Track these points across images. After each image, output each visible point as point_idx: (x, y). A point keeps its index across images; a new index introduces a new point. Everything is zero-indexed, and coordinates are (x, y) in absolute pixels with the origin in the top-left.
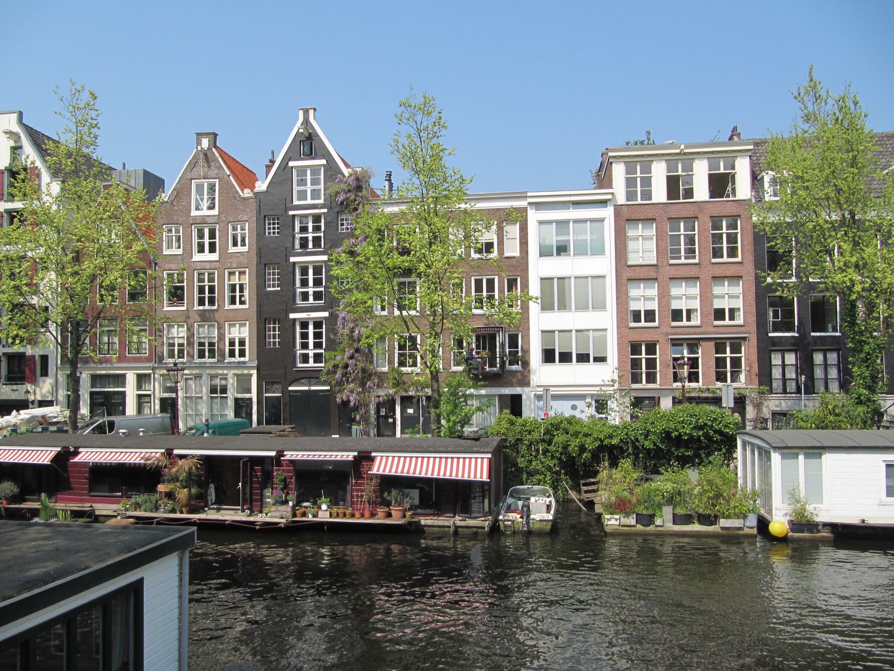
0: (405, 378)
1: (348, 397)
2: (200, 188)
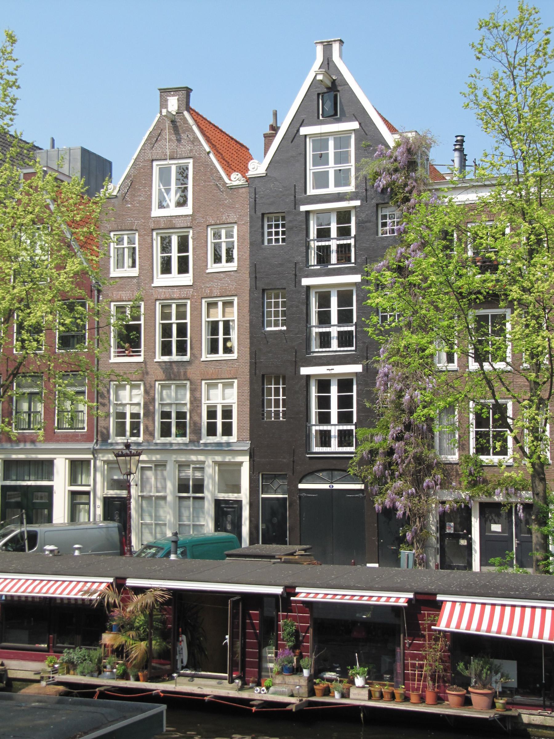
0: (487, 474)
1: (393, 502)
2: (165, 173)
